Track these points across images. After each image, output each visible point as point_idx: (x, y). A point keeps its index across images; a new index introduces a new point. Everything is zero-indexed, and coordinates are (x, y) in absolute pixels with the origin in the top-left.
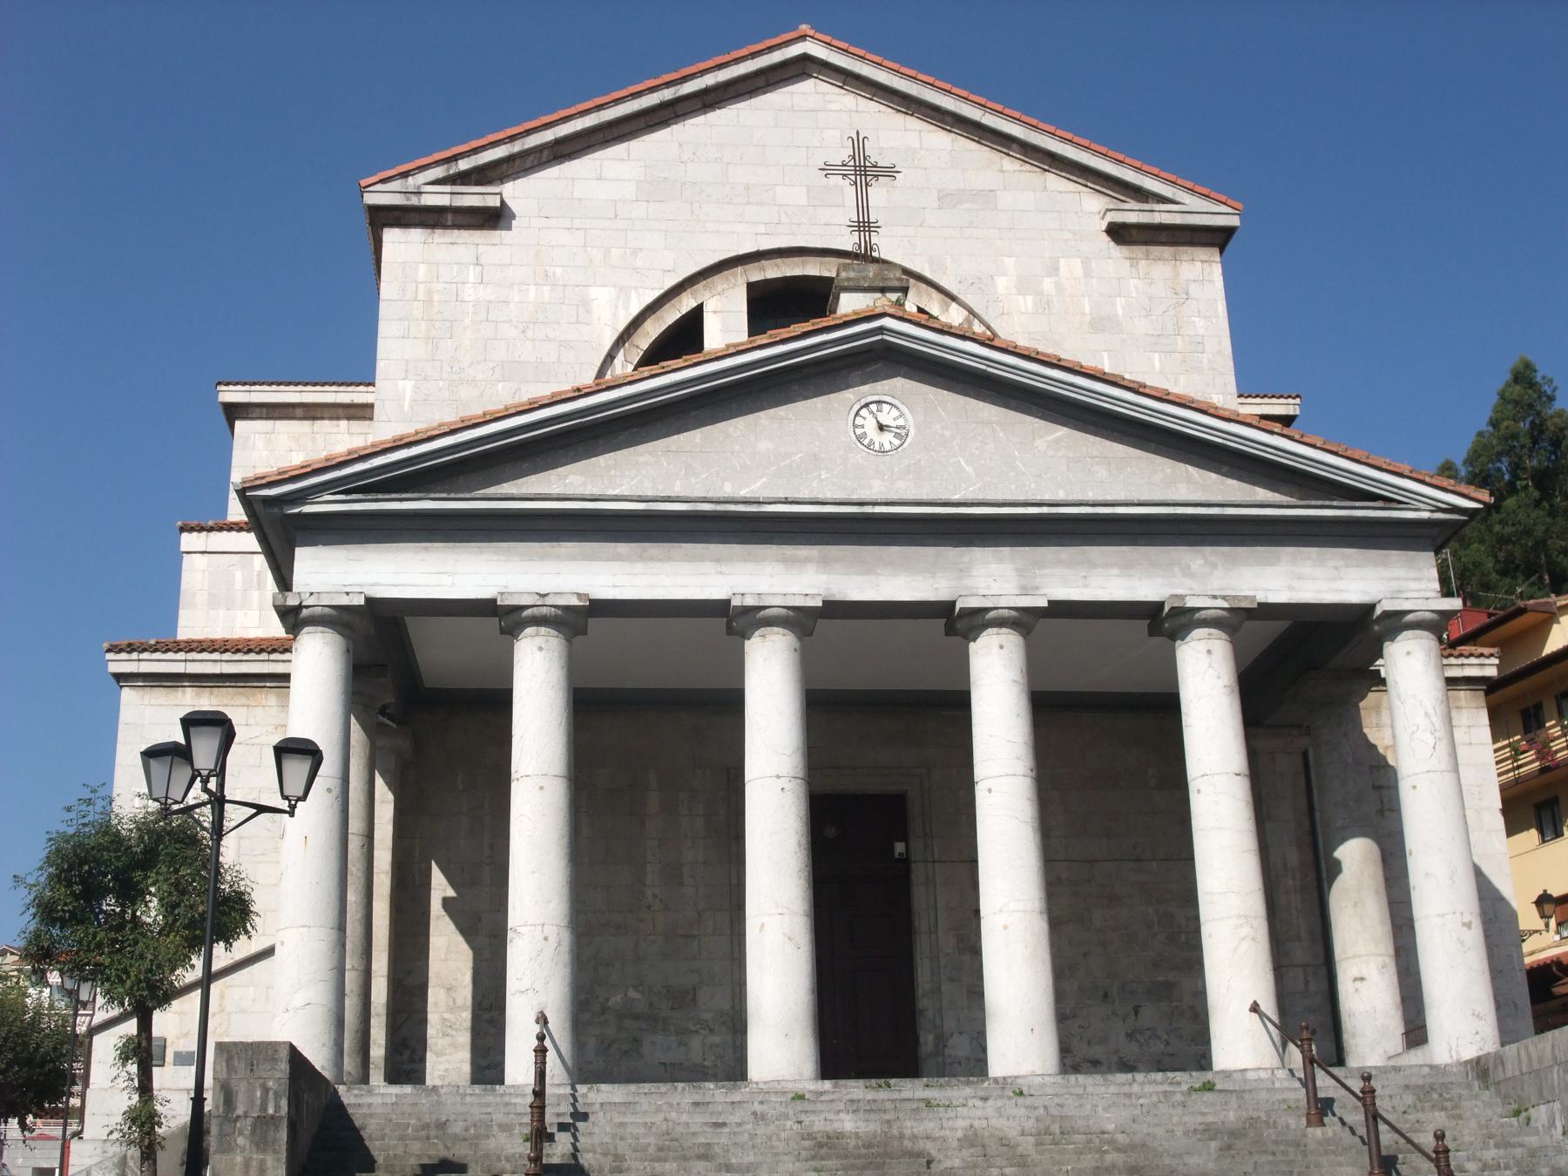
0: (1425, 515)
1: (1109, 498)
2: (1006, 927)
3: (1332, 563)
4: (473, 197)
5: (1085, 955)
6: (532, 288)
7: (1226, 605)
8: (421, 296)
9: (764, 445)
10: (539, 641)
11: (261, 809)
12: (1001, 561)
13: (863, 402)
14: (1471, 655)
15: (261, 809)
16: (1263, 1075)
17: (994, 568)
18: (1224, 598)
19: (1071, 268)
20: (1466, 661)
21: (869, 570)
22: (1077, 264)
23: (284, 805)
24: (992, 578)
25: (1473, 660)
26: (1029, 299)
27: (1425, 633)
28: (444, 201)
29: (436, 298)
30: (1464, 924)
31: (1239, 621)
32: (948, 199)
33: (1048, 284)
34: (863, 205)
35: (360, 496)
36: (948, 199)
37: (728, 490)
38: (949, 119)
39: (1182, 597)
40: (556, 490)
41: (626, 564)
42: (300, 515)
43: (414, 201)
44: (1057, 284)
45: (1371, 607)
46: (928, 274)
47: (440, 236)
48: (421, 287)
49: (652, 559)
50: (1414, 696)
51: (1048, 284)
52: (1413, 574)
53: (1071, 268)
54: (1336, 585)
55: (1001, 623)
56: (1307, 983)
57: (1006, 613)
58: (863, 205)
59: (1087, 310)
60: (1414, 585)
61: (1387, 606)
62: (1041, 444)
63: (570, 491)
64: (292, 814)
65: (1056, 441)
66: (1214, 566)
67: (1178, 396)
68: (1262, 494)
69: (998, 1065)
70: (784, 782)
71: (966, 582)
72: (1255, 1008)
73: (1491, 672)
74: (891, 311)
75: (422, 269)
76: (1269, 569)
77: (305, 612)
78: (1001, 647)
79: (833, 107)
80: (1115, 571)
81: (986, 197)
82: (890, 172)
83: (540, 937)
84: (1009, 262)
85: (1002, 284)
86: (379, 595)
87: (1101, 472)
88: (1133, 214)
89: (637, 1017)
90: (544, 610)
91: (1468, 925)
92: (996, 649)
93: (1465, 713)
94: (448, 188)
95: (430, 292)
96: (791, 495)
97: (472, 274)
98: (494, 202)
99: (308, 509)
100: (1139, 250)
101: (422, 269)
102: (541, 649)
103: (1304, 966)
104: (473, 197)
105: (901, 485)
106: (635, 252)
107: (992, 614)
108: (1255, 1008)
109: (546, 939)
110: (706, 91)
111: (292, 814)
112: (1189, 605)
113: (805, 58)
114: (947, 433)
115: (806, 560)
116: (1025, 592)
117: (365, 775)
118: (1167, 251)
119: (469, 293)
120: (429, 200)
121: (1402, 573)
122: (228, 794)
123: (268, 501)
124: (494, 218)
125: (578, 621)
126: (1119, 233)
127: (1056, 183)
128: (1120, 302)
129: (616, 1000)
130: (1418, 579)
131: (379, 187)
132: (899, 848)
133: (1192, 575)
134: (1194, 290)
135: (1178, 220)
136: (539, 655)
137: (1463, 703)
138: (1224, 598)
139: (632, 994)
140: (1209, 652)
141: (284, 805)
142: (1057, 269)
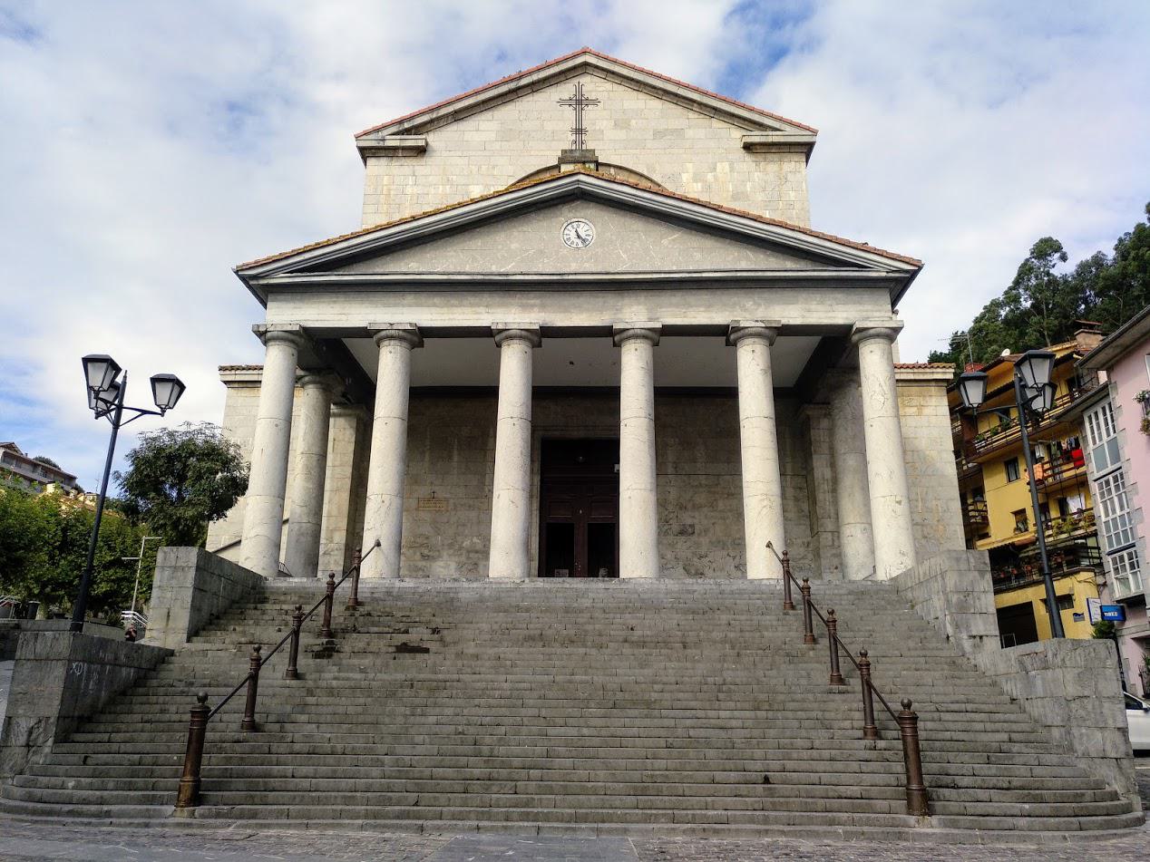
0: (884, 274)
1: (701, 268)
2: (630, 498)
3: (829, 303)
4: (412, 141)
5: (713, 524)
6: (441, 187)
7: (764, 325)
8: (384, 192)
9: (514, 246)
10: (390, 348)
11: (144, 412)
12: (639, 304)
13: (569, 222)
14: (938, 367)
15: (144, 412)
16: (772, 582)
17: (635, 308)
18: (762, 321)
19: (723, 167)
20: (934, 370)
21: (566, 310)
22: (726, 165)
23: (158, 410)
24: (635, 314)
25: (939, 370)
26: (700, 185)
27: (882, 340)
28: (396, 143)
29: (392, 192)
30: (897, 502)
31: (777, 334)
32: (658, 134)
33: (710, 177)
34: (579, 119)
35: (299, 274)
36: (658, 134)
37: (494, 269)
38: (660, 92)
39: (738, 321)
40: (404, 270)
41: (438, 309)
42: (267, 285)
43: (381, 144)
44: (716, 178)
45: (851, 326)
46: (646, 173)
47: (395, 162)
48: (385, 188)
49: (452, 306)
50: (873, 375)
51: (710, 177)
52: (877, 308)
53: (723, 167)
54: (830, 314)
55: (636, 337)
56: (833, 540)
57: (639, 331)
58: (579, 119)
59: (731, 189)
60: (877, 314)
61: (858, 325)
62: (665, 242)
63: (411, 271)
64: (162, 415)
65: (673, 240)
66: (760, 305)
67: (729, 209)
68: (789, 264)
69: (625, 570)
70: (515, 421)
71: (620, 316)
72: (769, 545)
73: (951, 376)
74: (583, 171)
75: (386, 178)
76: (791, 307)
77: (269, 335)
78: (636, 350)
79: (601, 89)
80: (702, 309)
81: (679, 133)
82: (595, 102)
83: (379, 500)
84: (690, 166)
85: (685, 177)
86: (308, 326)
87: (698, 256)
88: (757, 137)
89: (477, 552)
90: (393, 332)
91: (899, 503)
92: (633, 350)
93: (934, 399)
94: (398, 137)
95: (389, 190)
96: (524, 271)
97: (411, 180)
98: (421, 143)
99: (272, 281)
100: (760, 157)
101: (386, 178)
102: (391, 352)
103: (832, 532)
104: (412, 141)
105: (587, 265)
106: (494, 168)
107: (631, 332)
108: (769, 545)
109: (383, 502)
110: (533, 83)
111: (162, 415)
112: (742, 325)
113: (586, 64)
114: (614, 238)
115: (533, 306)
116: (650, 320)
117: (316, 420)
118: (776, 157)
119: (409, 190)
120: (388, 143)
121: (869, 307)
122: (125, 404)
123: (256, 277)
124: (421, 151)
125: (418, 337)
126: (748, 147)
127: (717, 124)
128: (749, 185)
129: (467, 543)
130: (880, 311)
131: (364, 137)
132: (616, 466)
133: (746, 310)
134: (790, 177)
135: (782, 140)
136: (389, 355)
137: (933, 393)
138: (762, 321)
139: (475, 540)
140: (753, 351)
141: (158, 410)
142: (715, 169)
